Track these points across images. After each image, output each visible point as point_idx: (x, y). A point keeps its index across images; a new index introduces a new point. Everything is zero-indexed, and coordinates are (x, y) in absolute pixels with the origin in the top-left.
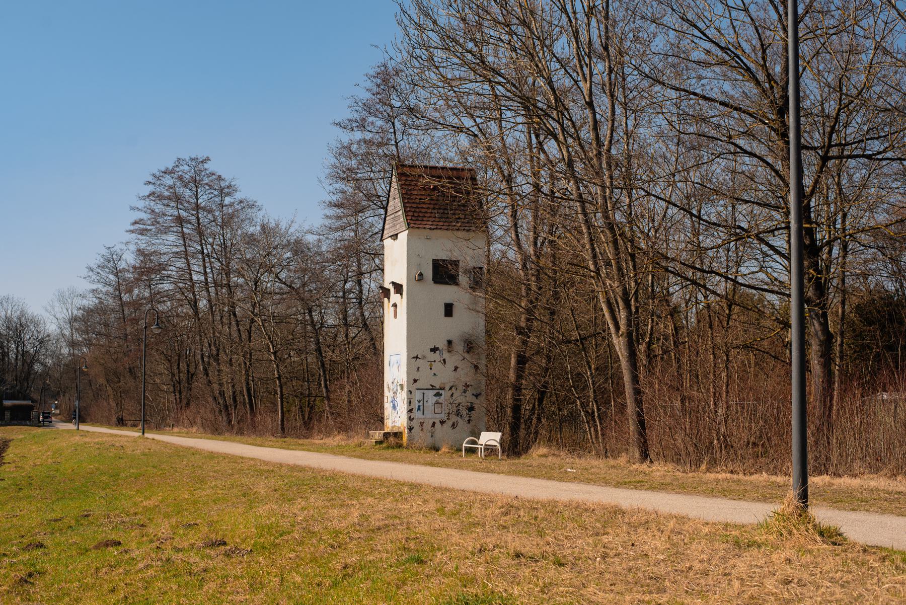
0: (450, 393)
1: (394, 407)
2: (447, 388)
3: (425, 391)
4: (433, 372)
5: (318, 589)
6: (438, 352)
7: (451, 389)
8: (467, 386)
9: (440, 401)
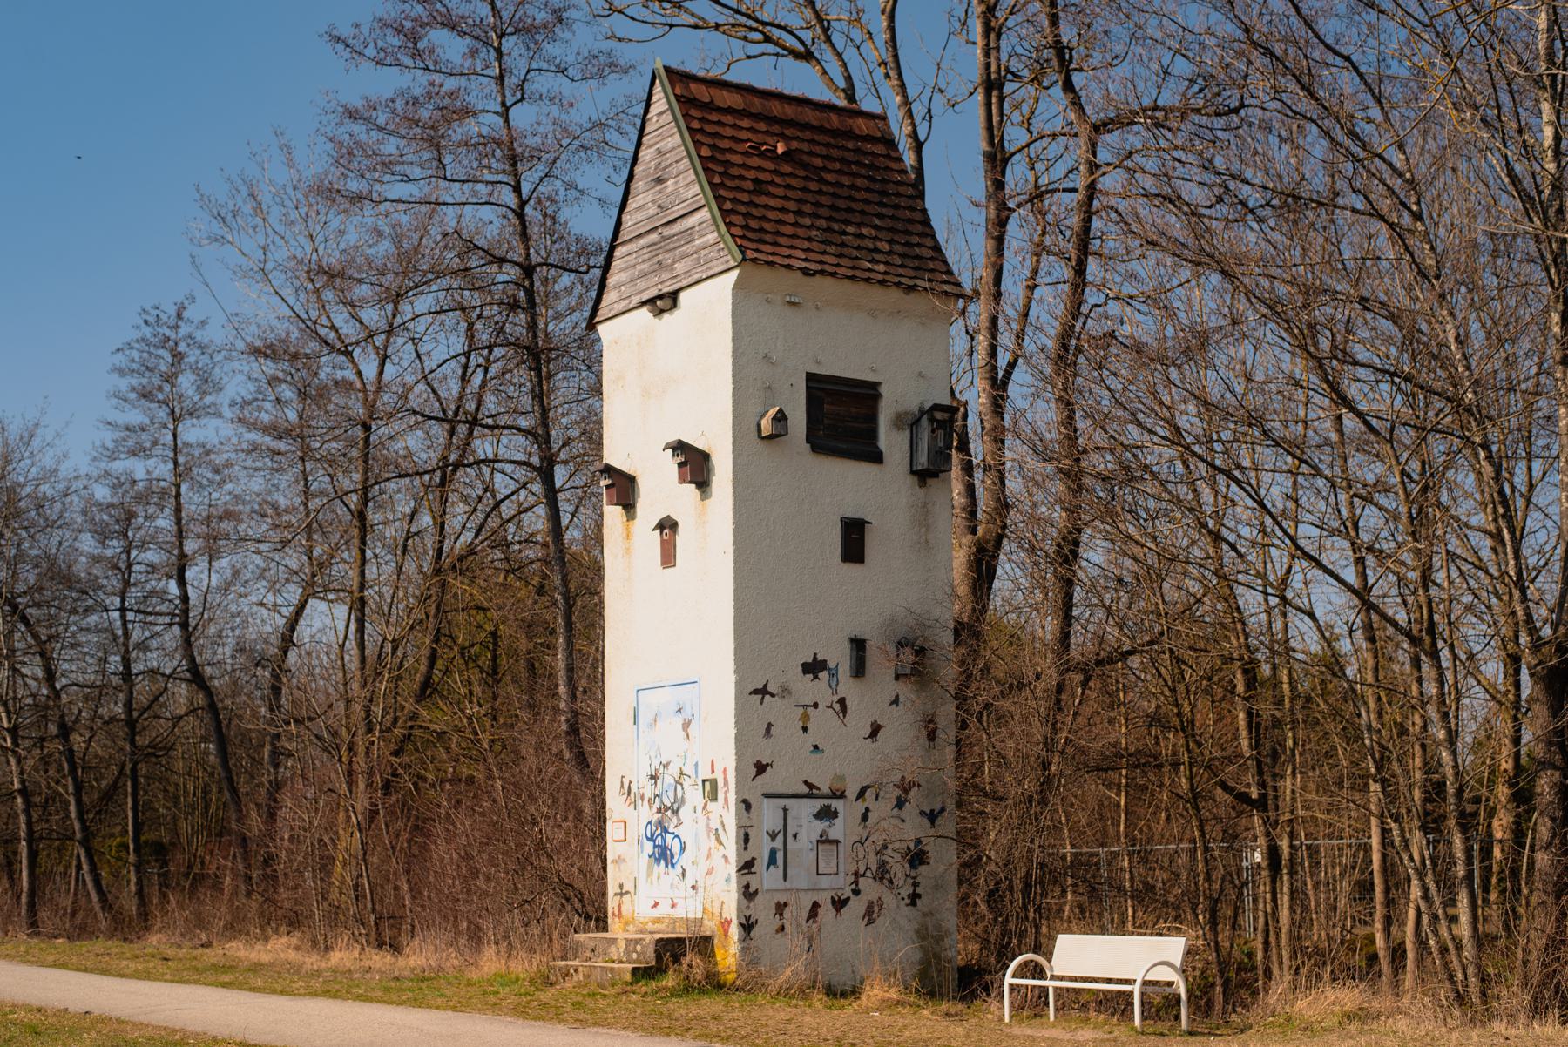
0: (860, 807)
1: (663, 855)
2: (852, 793)
6: (824, 675)
7: (861, 794)
9: (833, 835)
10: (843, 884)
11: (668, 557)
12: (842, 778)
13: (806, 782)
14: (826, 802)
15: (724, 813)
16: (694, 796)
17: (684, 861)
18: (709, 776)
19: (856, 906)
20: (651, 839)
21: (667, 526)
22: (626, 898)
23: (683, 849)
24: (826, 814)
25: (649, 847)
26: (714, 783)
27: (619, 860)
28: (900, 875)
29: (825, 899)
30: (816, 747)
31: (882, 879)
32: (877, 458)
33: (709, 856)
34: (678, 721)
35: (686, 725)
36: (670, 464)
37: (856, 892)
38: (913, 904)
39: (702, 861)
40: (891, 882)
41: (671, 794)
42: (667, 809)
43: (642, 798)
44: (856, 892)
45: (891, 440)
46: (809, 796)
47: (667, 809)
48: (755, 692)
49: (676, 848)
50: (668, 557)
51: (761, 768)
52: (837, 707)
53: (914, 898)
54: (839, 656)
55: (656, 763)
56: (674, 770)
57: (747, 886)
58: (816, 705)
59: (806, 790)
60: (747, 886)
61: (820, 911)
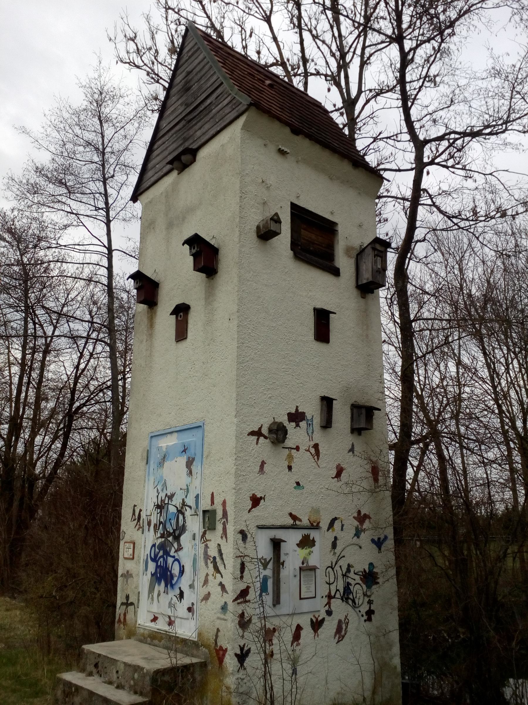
0: (330, 536)
1: (164, 576)
2: (324, 525)
3: (279, 534)
4: (294, 477)
5: (501, 87)
6: (303, 424)
7: (331, 525)
8: (361, 518)
9: (313, 561)
10: (319, 605)
11: (181, 334)
12: (316, 511)
13: (291, 514)
14: (306, 532)
15: (223, 542)
16: (194, 525)
17: (184, 583)
18: (209, 508)
19: (329, 628)
20: (154, 560)
21: (182, 311)
22: (131, 608)
23: (182, 572)
24: (306, 543)
25: (152, 566)
26: (213, 513)
27: (128, 575)
28: (360, 594)
29: (305, 621)
30: (298, 484)
31: (347, 599)
32: (336, 272)
33: (206, 582)
34: (182, 460)
35: (189, 463)
36: (185, 258)
37: (329, 613)
38: (369, 619)
39: (198, 584)
40: (354, 601)
41: (174, 522)
42: (169, 534)
43: (149, 524)
44: (329, 613)
45: (344, 262)
46: (293, 527)
47: (169, 534)
48: (252, 433)
49: (176, 570)
50: (181, 334)
51: (256, 501)
52: (313, 451)
53: (370, 613)
54: (312, 410)
55: (162, 495)
56: (177, 501)
57: (242, 615)
58: (297, 448)
59: (290, 521)
60: (242, 615)
61: (303, 633)
